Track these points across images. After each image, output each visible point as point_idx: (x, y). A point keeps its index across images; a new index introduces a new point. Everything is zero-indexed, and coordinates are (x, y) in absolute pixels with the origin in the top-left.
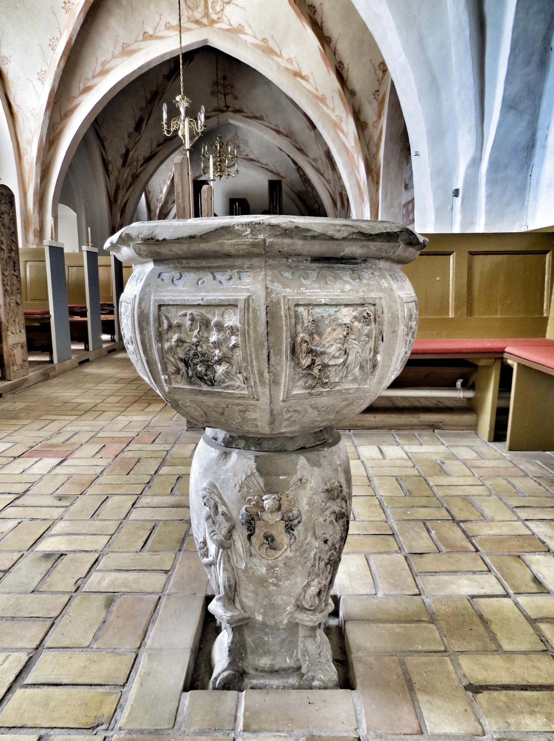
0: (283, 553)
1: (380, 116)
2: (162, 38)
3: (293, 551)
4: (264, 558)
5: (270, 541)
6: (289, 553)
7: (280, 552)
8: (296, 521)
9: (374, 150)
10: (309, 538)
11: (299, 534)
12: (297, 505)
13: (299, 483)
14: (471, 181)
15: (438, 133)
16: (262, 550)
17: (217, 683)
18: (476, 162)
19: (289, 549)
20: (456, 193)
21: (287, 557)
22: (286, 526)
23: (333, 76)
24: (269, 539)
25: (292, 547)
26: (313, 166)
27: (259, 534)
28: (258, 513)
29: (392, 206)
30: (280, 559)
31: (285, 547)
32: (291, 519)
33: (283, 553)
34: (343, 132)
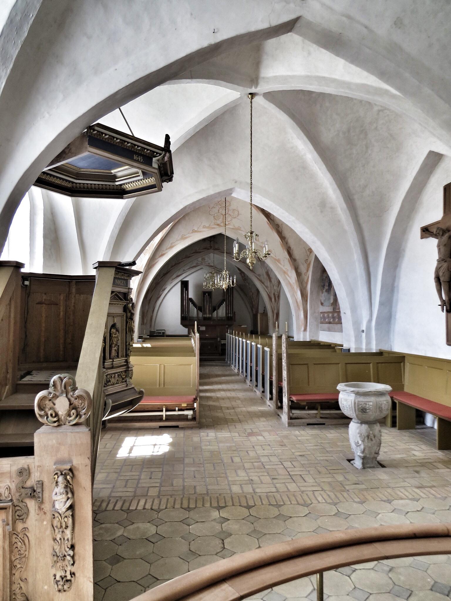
1: (308, 271)
2: (201, 231)
5: (372, 440)
9: (305, 285)
14: (369, 327)
15: (354, 309)
18: (370, 321)
20: (363, 331)
23: (286, 253)
26: (258, 279)
29: (315, 312)
34: (289, 276)
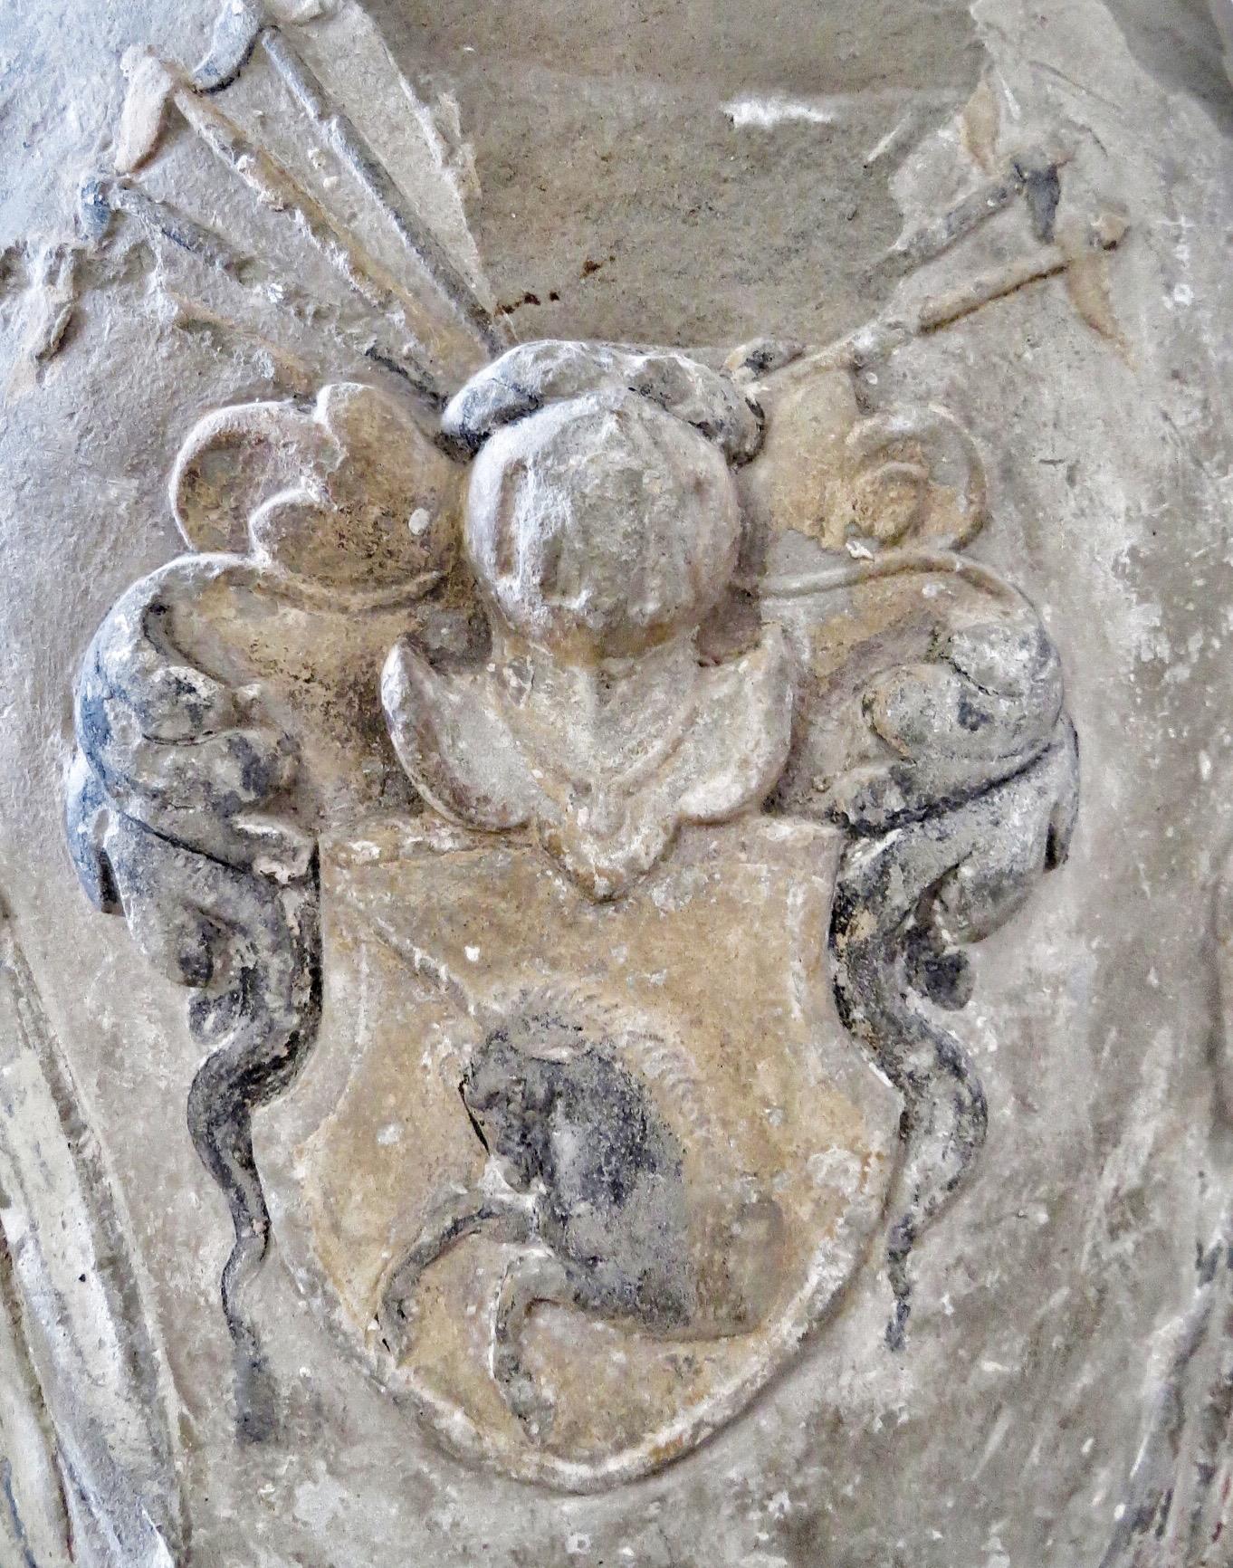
0: (787, 1367)
3: (930, 1323)
4: (476, 1466)
6: (873, 1372)
7: (751, 1360)
8: (1018, 820)
10: (1143, 1132)
11: (1024, 1051)
12: (999, 557)
13: (1015, 221)
16: (438, 1333)
17: (292, 922)
19: (876, 1305)
21: (830, 1423)
22: (840, 919)
24: (567, 1142)
25: (917, 1269)
27: (399, 1047)
28: (369, 693)
30: (733, 1463)
31: (823, 1273)
32: (940, 774)
33: (787, 1367)
